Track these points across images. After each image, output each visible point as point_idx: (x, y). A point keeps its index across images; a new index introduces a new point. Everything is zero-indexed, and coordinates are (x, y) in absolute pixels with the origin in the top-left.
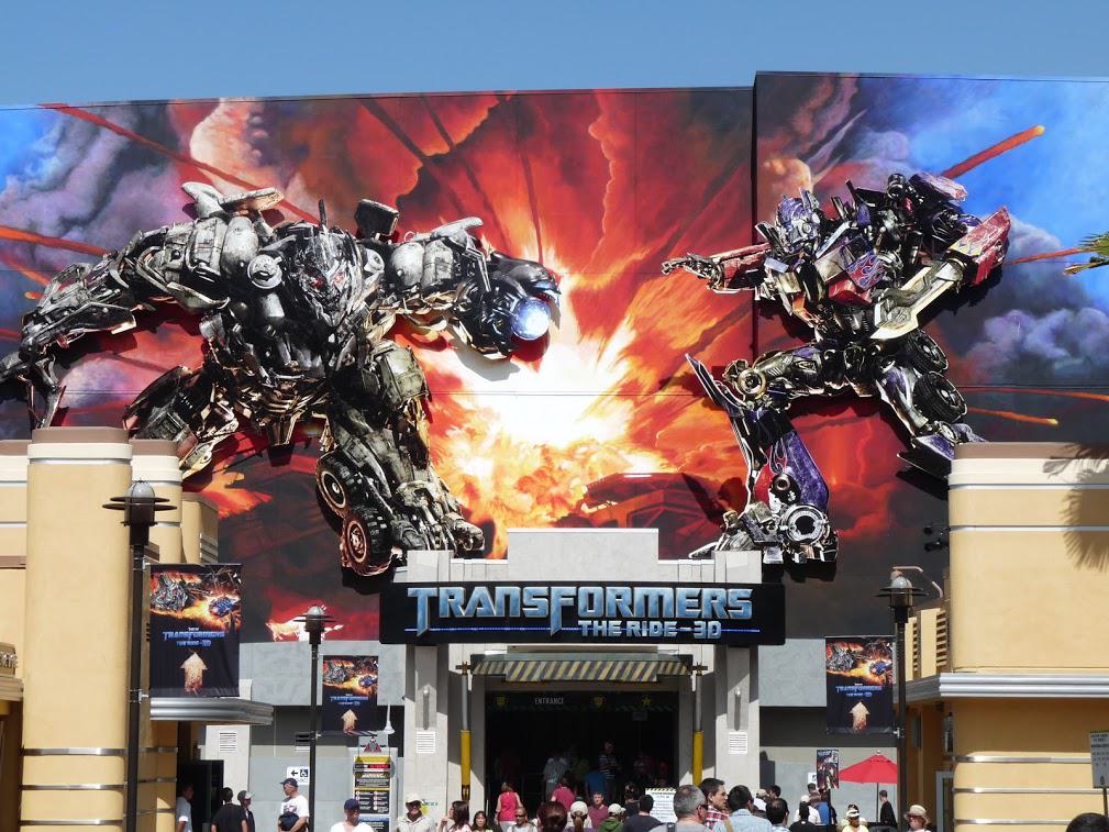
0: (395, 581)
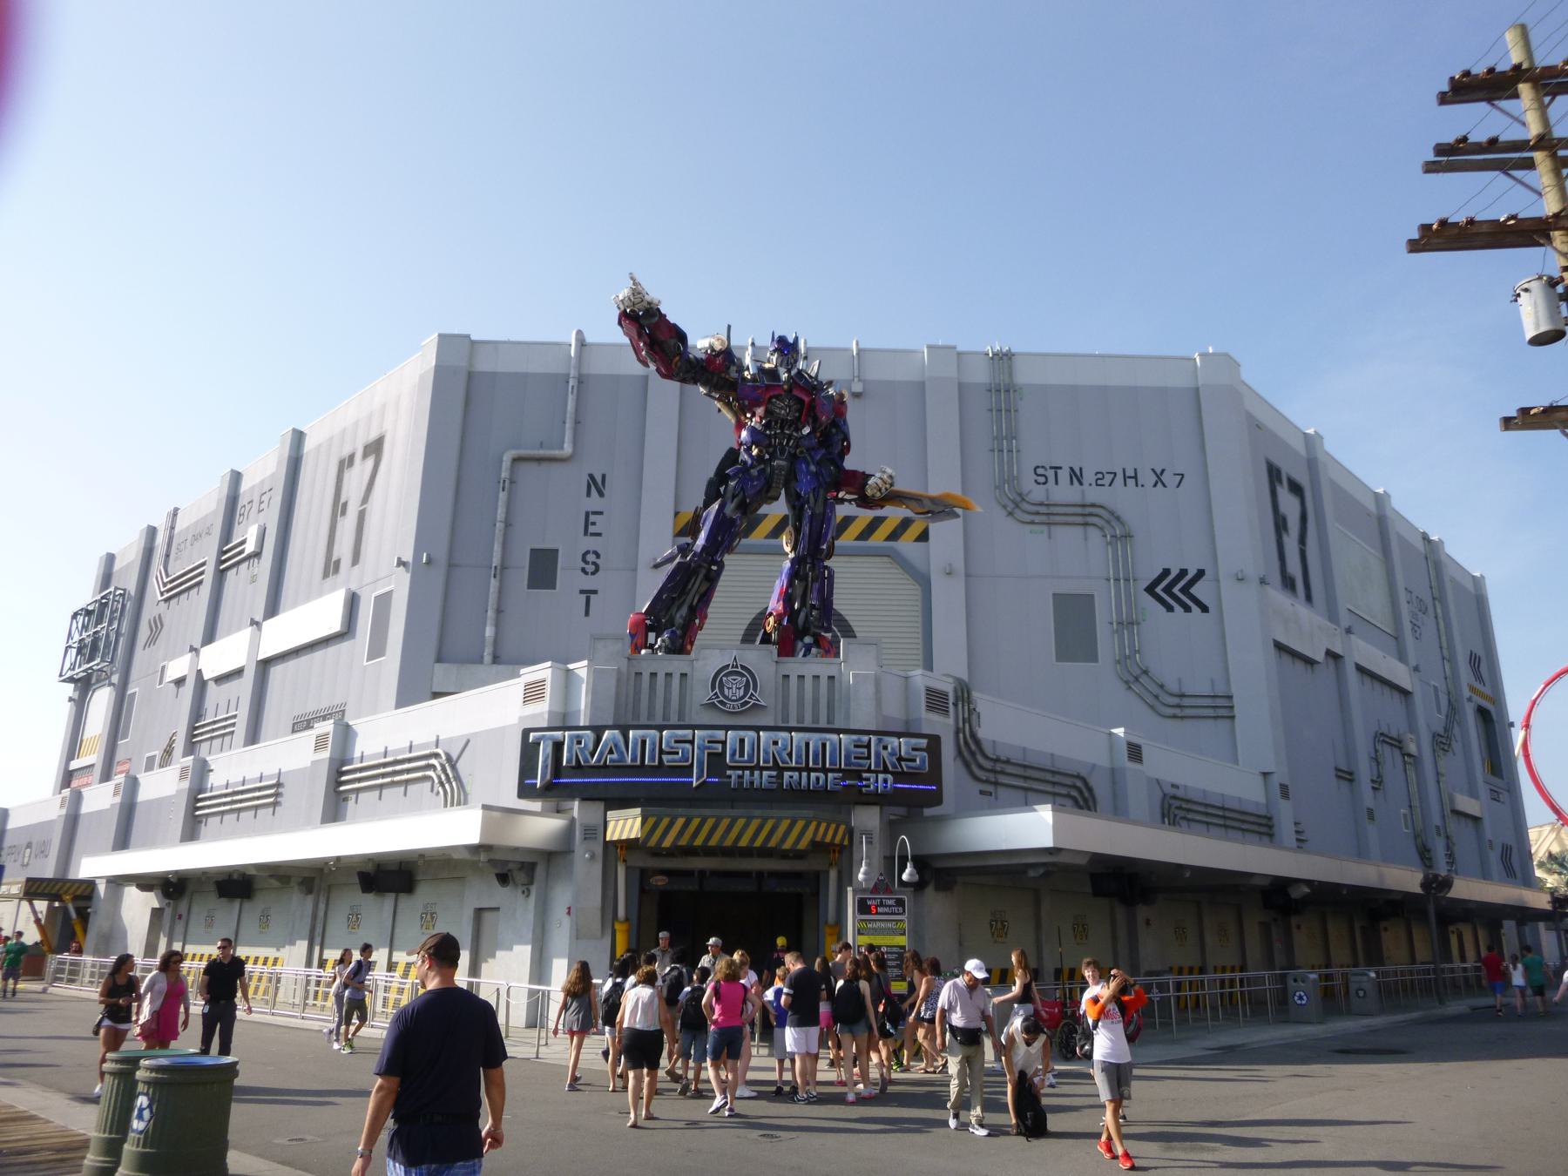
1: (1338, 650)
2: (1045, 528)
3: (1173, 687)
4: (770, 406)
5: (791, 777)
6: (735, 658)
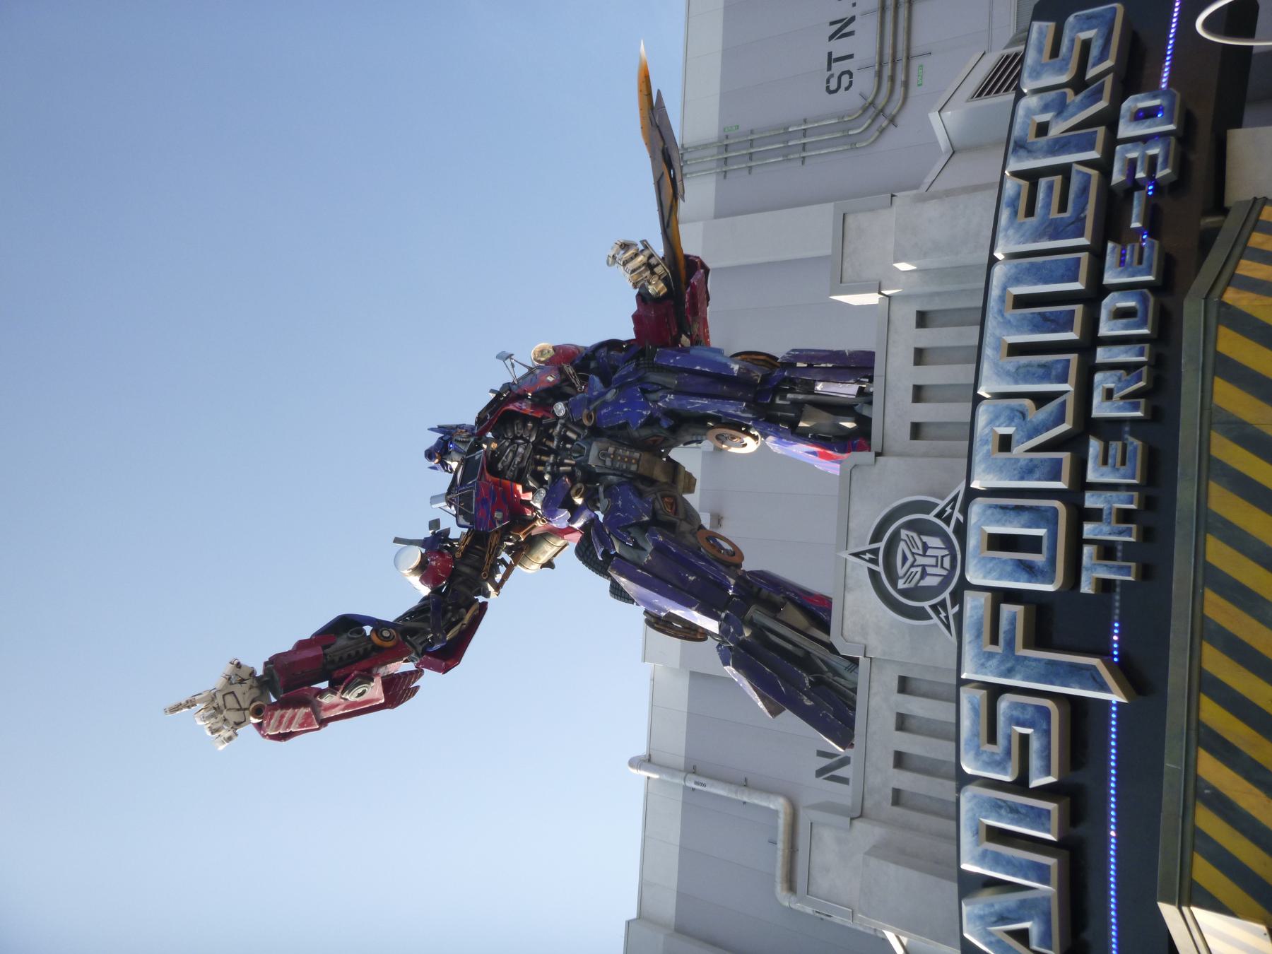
0: (327, 682)
2: (915, 64)
4: (509, 474)
5: (1109, 394)
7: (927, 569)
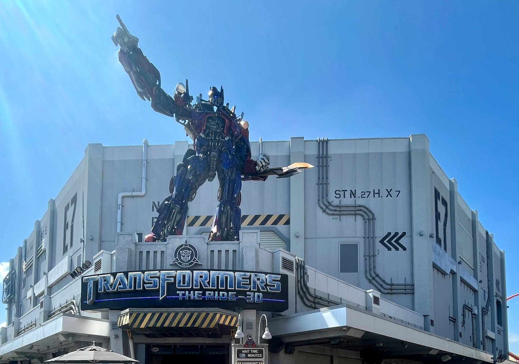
1: (455, 270)
2: (338, 217)
3: (389, 282)
4: (208, 124)
5: (210, 294)
6: (186, 241)
7: (184, 257)
